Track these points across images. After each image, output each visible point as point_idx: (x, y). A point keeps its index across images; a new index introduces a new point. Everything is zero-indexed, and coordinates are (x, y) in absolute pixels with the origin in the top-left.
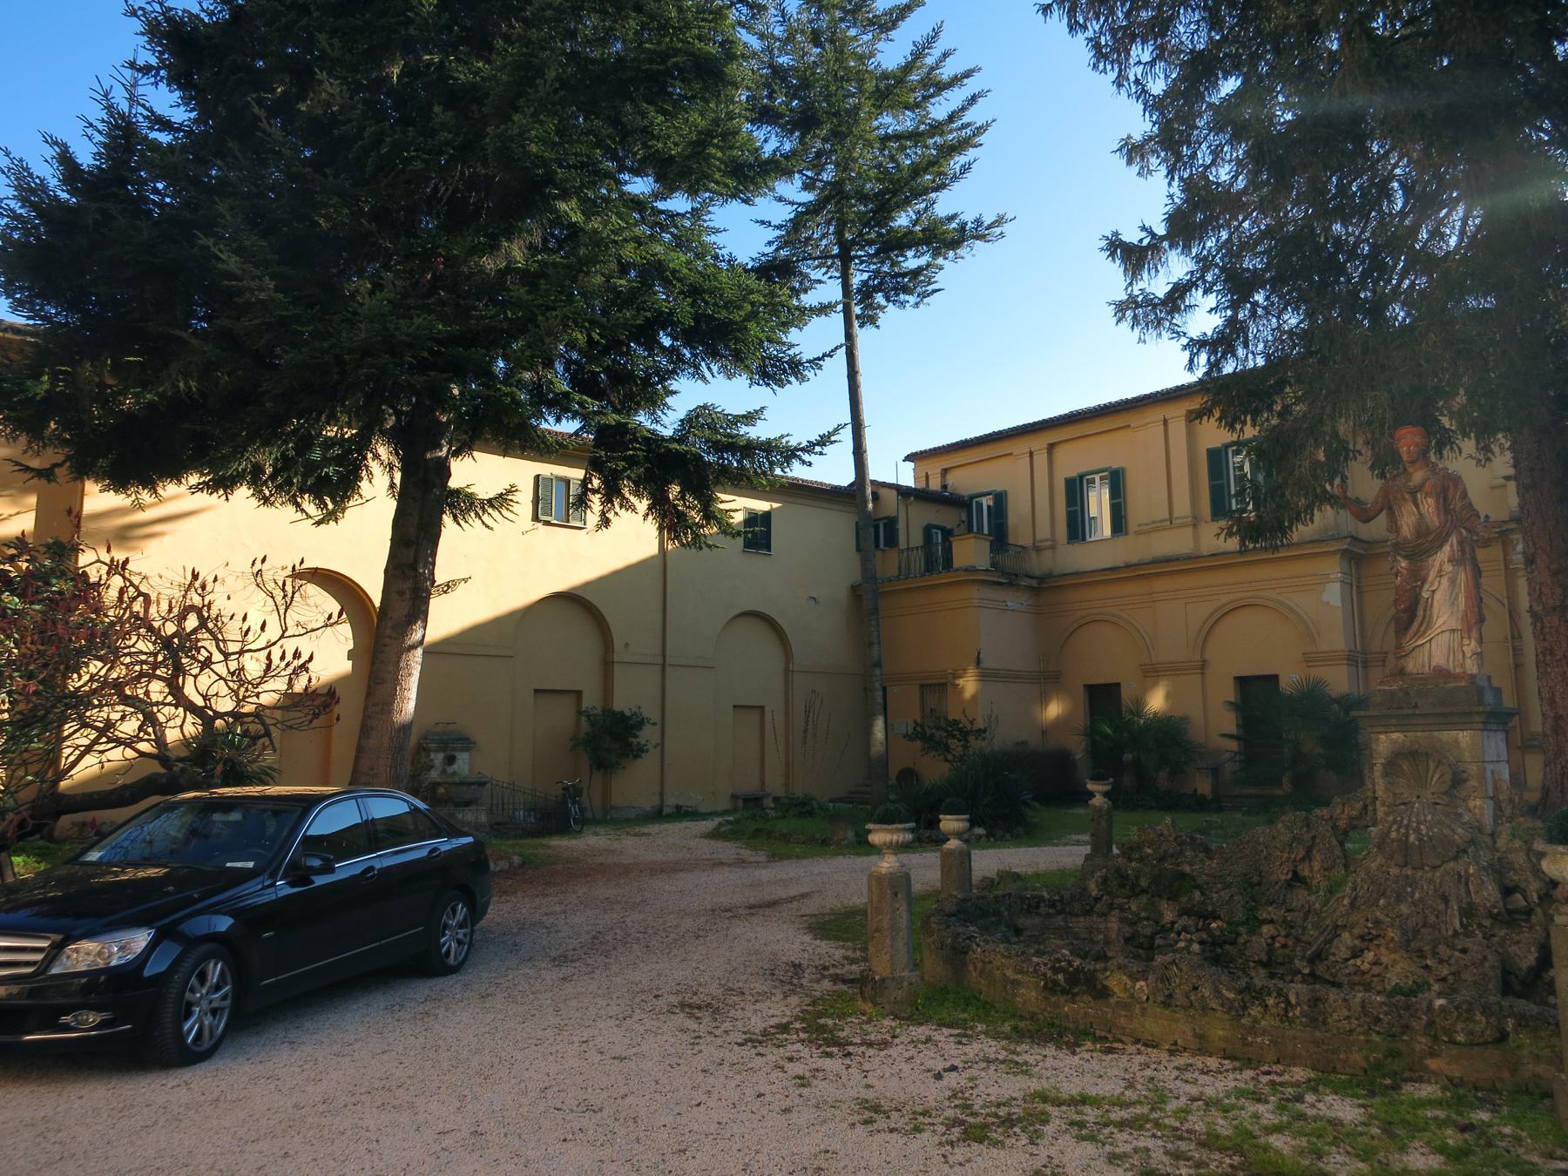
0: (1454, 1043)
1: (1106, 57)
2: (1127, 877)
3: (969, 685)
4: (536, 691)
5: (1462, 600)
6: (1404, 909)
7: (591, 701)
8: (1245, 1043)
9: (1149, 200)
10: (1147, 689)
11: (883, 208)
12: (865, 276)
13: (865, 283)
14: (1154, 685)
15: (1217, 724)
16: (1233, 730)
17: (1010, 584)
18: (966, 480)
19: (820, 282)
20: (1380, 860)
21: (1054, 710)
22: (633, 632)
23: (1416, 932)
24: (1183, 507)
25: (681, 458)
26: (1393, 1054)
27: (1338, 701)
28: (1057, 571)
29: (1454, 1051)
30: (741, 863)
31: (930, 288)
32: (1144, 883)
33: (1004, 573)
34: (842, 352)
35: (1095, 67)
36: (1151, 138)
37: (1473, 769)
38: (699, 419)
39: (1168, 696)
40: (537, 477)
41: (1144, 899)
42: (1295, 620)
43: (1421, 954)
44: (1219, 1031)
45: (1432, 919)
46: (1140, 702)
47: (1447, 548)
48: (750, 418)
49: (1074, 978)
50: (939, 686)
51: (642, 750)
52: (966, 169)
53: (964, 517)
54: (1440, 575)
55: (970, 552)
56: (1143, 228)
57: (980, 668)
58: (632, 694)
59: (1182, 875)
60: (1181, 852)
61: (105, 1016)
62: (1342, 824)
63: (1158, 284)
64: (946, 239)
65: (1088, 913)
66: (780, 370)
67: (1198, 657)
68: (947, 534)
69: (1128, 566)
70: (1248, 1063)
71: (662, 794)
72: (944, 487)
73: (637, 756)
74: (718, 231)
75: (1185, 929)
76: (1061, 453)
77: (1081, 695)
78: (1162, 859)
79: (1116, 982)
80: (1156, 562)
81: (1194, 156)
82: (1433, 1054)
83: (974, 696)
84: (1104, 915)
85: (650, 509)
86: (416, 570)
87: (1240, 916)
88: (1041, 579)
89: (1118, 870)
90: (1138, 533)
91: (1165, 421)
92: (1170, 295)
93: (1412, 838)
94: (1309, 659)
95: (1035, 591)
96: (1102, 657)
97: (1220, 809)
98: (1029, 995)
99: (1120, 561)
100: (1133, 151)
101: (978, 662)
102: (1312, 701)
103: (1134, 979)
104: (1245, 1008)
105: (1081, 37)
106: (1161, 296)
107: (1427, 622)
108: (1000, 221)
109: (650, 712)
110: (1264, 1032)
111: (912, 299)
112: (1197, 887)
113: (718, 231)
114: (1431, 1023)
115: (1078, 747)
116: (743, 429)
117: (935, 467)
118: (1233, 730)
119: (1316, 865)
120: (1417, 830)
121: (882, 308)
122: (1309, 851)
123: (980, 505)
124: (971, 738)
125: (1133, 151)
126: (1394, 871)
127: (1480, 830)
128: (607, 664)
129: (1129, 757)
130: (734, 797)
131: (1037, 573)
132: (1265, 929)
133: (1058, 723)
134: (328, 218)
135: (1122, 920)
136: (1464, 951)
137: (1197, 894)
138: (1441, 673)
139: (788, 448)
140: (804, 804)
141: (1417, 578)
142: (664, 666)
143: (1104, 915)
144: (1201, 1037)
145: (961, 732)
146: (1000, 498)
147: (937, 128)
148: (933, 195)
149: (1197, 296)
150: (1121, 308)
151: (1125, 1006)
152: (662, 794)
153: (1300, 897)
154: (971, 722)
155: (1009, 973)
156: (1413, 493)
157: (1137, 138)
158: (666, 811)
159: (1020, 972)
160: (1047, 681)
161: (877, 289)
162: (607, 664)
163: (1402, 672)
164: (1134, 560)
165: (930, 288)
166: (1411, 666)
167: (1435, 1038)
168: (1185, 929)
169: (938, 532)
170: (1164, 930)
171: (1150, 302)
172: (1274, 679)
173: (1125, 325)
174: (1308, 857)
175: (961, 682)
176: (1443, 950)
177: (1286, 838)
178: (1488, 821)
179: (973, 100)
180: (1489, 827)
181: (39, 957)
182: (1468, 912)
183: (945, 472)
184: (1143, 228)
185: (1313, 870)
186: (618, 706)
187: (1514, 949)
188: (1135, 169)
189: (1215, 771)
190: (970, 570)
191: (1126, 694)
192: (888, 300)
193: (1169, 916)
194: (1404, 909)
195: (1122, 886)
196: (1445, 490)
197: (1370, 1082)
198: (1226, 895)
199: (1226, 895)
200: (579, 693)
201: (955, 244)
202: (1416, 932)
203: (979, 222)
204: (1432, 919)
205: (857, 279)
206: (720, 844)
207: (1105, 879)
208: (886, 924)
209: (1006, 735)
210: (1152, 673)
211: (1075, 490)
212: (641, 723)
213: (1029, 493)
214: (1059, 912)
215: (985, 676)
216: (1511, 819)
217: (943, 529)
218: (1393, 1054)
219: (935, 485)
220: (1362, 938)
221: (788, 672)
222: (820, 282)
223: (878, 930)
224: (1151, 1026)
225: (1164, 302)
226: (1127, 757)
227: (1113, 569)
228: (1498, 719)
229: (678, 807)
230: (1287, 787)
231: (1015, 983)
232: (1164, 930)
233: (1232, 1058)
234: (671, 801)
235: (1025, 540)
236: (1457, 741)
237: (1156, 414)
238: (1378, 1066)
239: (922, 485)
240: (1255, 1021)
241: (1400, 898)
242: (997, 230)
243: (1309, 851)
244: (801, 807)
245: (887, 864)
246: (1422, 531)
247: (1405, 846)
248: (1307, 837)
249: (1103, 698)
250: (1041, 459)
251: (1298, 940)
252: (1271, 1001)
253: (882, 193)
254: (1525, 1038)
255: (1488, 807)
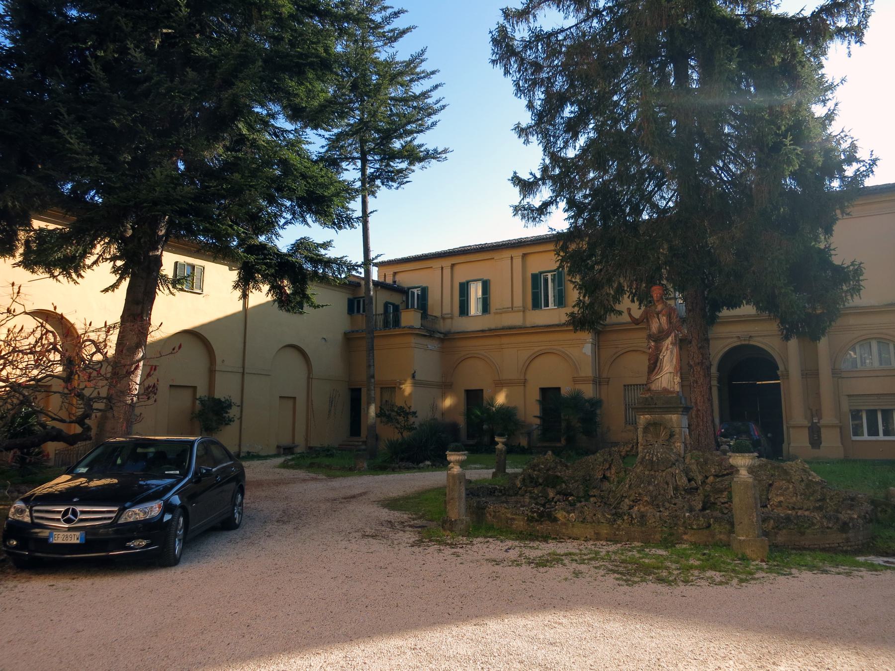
0: (692, 529)
1: (523, 92)
2: (533, 478)
3: (407, 388)
4: (171, 386)
5: (674, 360)
6: (651, 488)
7: (202, 392)
8: (615, 534)
9: (531, 158)
10: (496, 393)
11: (387, 136)
12: (372, 170)
13: (372, 173)
14: (500, 390)
15: (530, 411)
16: (538, 414)
17: (430, 336)
18: (407, 279)
19: (347, 170)
20: (641, 468)
21: (448, 402)
22: (227, 353)
23: (656, 497)
24: (518, 302)
25: (293, 265)
26: (671, 534)
27: (587, 401)
28: (453, 331)
29: (693, 531)
30: (313, 479)
31: (405, 180)
32: (540, 481)
33: (428, 331)
34: (369, 210)
35: (516, 95)
36: (531, 127)
37: (677, 430)
38: (301, 245)
39: (507, 396)
40: (176, 263)
41: (540, 488)
42: (571, 362)
43: (658, 506)
44: (605, 530)
45: (662, 492)
46: (493, 399)
47: (670, 338)
48: (326, 245)
49: (541, 515)
50: (393, 388)
51: (230, 421)
52: (434, 124)
53: (404, 299)
54: (667, 349)
55: (410, 318)
56: (531, 174)
57: (414, 380)
58: (225, 389)
59: (558, 477)
60: (556, 467)
61: (148, 541)
62: (623, 454)
63: (536, 201)
64: (414, 156)
65: (516, 494)
66: (342, 221)
67: (522, 377)
68: (396, 308)
69: (490, 330)
70: (616, 542)
71: (240, 446)
72: (395, 282)
73: (227, 424)
74: (310, 143)
75: (559, 500)
76: (457, 268)
77: (463, 395)
78: (548, 470)
79: (560, 515)
80: (503, 329)
81: (555, 143)
82: (685, 533)
83: (410, 394)
84: (523, 496)
85: (270, 290)
86: (142, 317)
87: (581, 494)
88: (445, 334)
89: (529, 475)
90: (496, 313)
91: (512, 258)
92: (540, 207)
93: (655, 459)
94: (575, 380)
95: (442, 340)
96: (475, 376)
97: (531, 453)
98: (520, 524)
99: (486, 327)
100: (522, 132)
101: (413, 377)
102: (576, 400)
103: (569, 513)
104: (615, 521)
105: (509, 78)
106: (537, 206)
107: (661, 369)
108: (445, 151)
109: (236, 400)
110: (623, 530)
111: (395, 185)
112: (564, 482)
113: (310, 143)
114: (684, 522)
115: (461, 421)
116: (323, 252)
117: (389, 271)
118: (538, 414)
119: (613, 471)
120: (657, 455)
121: (378, 187)
122: (610, 465)
123: (413, 293)
124: (410, 416)
125: (522, 132)
126: (647, 473)
127: (679, 455)
128: (212, 372)
129: (481, 427)
130: (278, 447)
131: (443, 331)
132: (592, 499)
133: (450, 409)
134: (118, 121)
135: (531, 498)
136: (675, 504)
137: (564, 485)
138: (665, 390)
139: (350, 264)
140: (328, 450)
141: (658, 349)
142: (243, 374)
143: (523, 496)
144: (597, 534)
145: (405, 412)
146: (424, 290)
147: (415, 98)
148: (415, 135)
149: (552, 208)
150: (516, 209)
151: (565, 524)
152: (240, 446)
153: (606, 485)
154: (409, 408)
155: (509, 515)
156: (658, 314)
157: (524, 125)
158: (242, 455)
159: (516, 514)
160: (446, 387)
161: (377, 177)
162: (212, 372)
163: (649, 390)
164: (493, 327)
165: (405, 180)
166: (654, 387)
167: (686, 528)
168: (559, 500)
169: (387, 304)
170: (549, 501)
171: (530, 209)
172: (559, 389)
173: (519, 217)
174: (610, 468)
175: (403, 386)
176: (667, 505)
177: (601, 460)
178: (682, 452)
179: (436, 87)
180: (682, 455)
181: (113, 515)
182: (676, 488)
183: (395, 274)
184: (531, 174)
185: (612, 474)
186: (217, 396)
187: (693, 503)
188: (522, 140)
189: (529, 434)
190: (411, 328)
191: (486, 395)
192: (383, 184)
193: (551, 495)
194: (651, 488)
195: (531, 482)
196: (670, 314)
197: (667, 543)
198: (576, 485)
199: (576, 485)
200: (195, 388)
201: (421, 160)
202: (656, 497)
203: (435, 150)
204: (662, 492)
205: (369, 171)
206: (283, 471)
207: (524, 480)
208: (456, 496)
209: (423, 414)
210: (500, 384)
211: (464, 289)
212: (230, 406)
213: (439, 288)
214: (504, 495)
215: (417, 384)
216: (690, 451)
217: (393, 305)
218: (671, 534)
219: (389, 280)
220: (633, 501)
221: (309, 378)
222: (347, 170)
223: (452, 499)
224: (576, 531)
225: (537, 210)
226: (485, 427)
227: (483, 331)
228: (686, 410)
229: (248, 453)
230: (563, 442)
231: (513, 519)
232: (549, 501)
233: (611, 541)
234: (245, 449)
235: (438, 314)
236: (671, 419)
237: (507, 254)
238: (666, 539)
239: (382, 280)
240: (619, 526)
241: (649, 483)
242: (444, 156)
243: (610, 465)
244: (328, 452)
245: (456, 470)
246: (661, 330)
247: (652, 462)
248: (610, 459)
249: (474, 397)
250: (447, 272)
251: (605, 503)
252: (626, 518)
253: (388, 130)
254: (717, 526)
255: (682, 446)
